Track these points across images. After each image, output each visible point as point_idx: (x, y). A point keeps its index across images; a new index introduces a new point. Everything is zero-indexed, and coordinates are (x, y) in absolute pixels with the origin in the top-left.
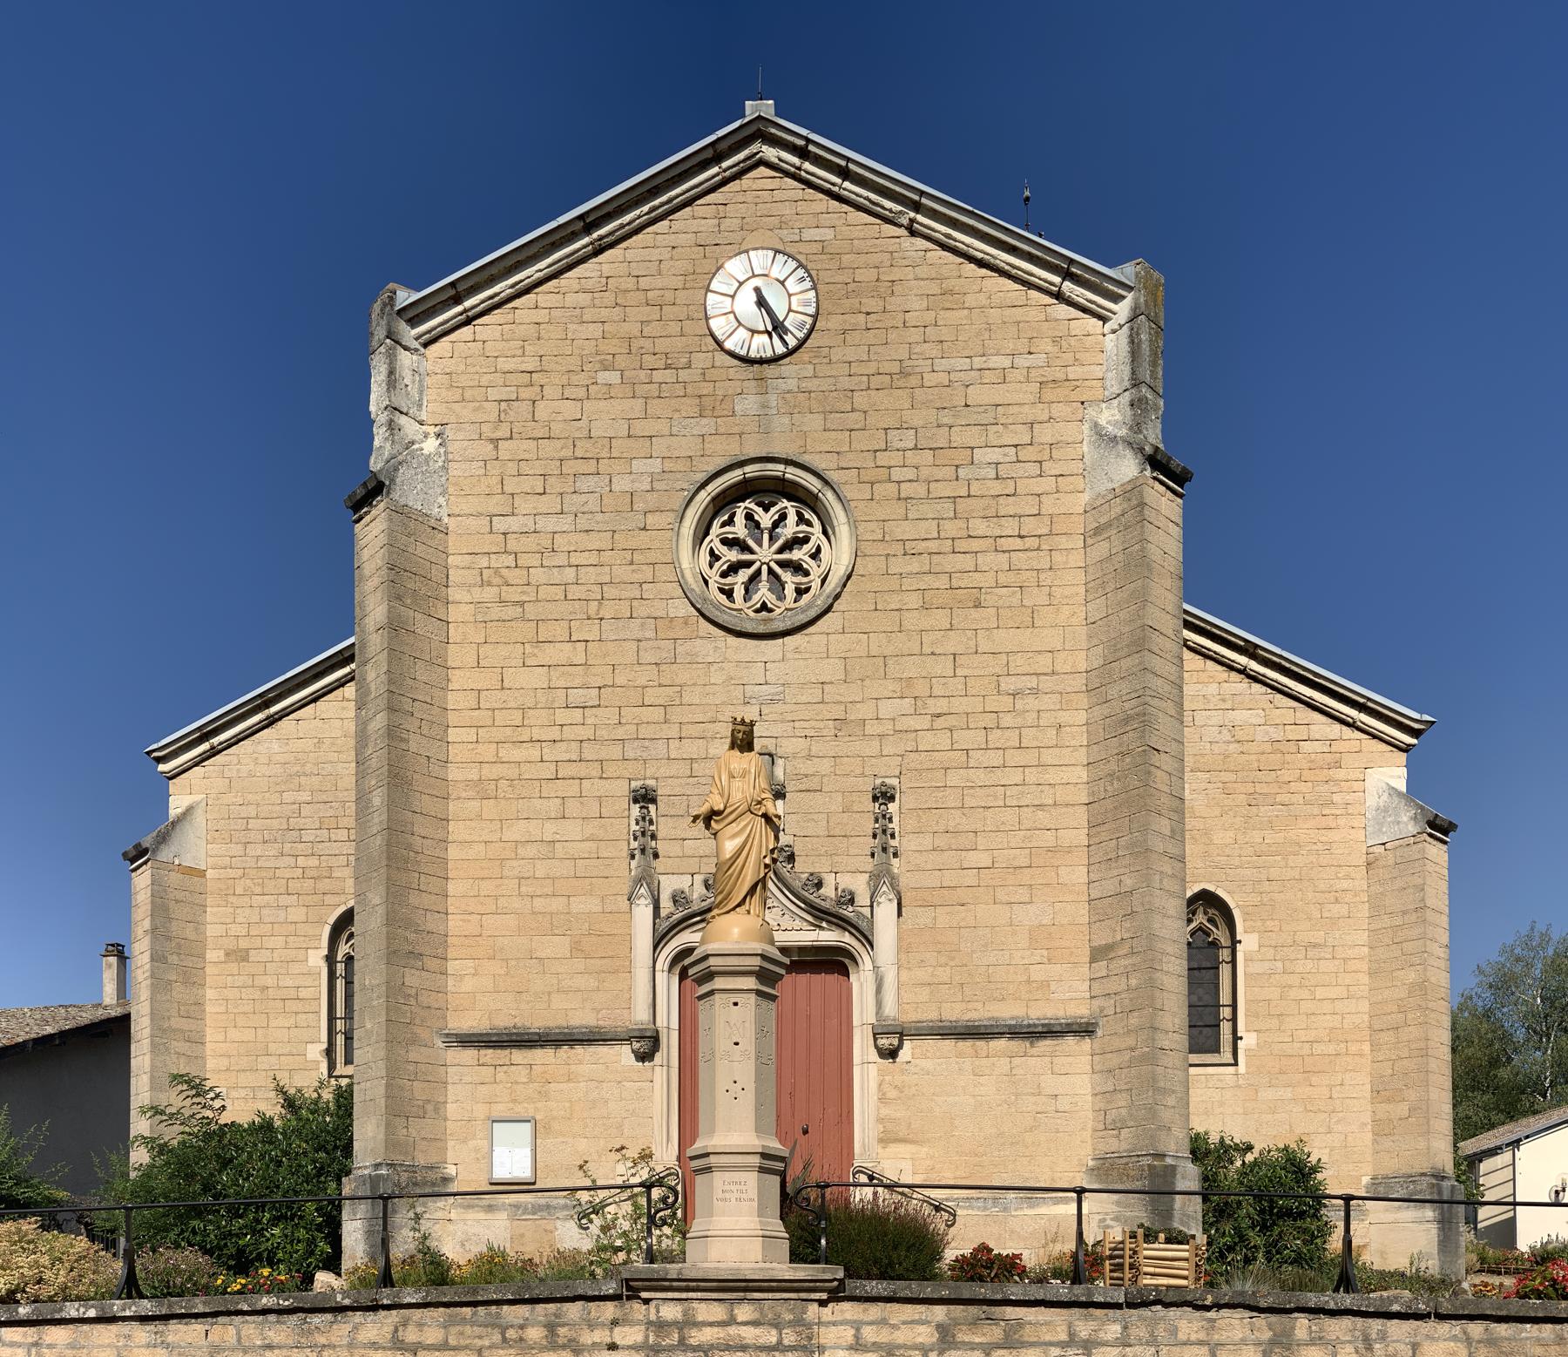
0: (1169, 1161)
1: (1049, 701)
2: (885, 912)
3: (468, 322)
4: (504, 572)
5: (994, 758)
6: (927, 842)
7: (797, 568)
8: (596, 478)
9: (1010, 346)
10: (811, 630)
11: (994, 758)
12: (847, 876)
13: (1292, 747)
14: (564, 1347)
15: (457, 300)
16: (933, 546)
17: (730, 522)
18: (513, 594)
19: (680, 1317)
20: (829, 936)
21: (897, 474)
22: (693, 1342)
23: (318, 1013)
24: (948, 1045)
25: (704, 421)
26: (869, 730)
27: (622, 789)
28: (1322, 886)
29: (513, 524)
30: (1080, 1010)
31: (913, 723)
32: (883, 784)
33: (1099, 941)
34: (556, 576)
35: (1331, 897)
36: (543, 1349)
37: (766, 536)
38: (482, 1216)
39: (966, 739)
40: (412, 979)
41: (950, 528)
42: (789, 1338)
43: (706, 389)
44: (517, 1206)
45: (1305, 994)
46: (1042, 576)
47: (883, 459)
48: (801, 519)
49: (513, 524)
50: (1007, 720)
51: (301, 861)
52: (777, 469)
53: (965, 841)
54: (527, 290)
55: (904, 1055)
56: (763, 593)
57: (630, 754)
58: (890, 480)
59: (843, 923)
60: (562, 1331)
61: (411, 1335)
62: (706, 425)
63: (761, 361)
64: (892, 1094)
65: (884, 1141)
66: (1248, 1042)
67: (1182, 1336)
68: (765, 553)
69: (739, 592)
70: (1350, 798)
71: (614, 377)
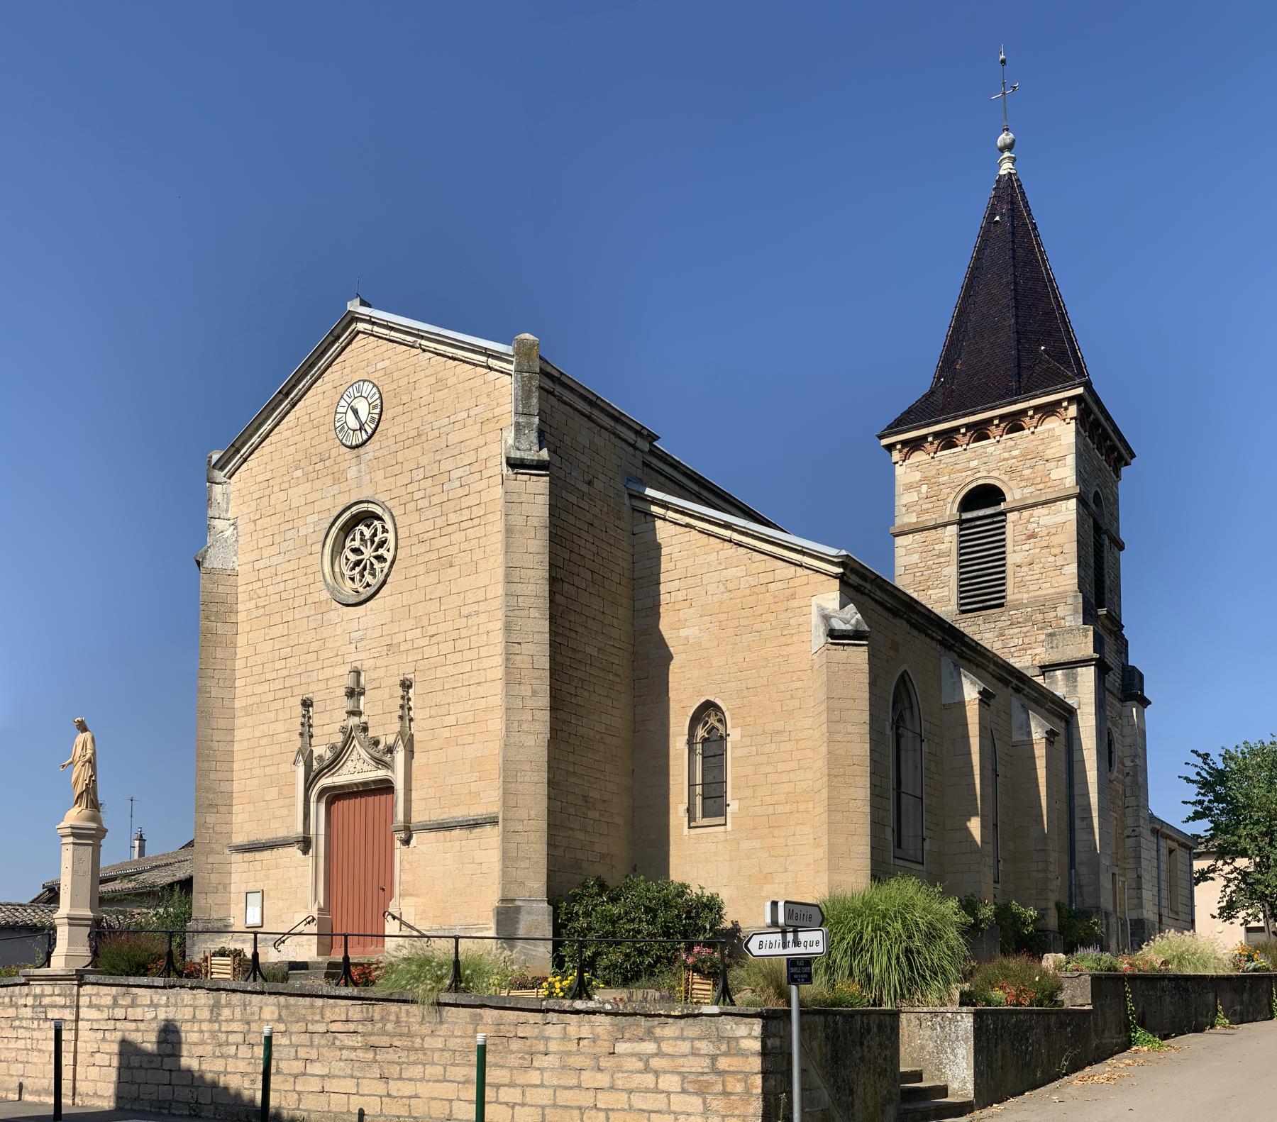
0: (518, 903)
1: (484, 617)
3: (245, 460)
6: (427, 713)
9: (467, 404)
13: (763, 589)
15: (238, 451)
16: (431, 535)
17: (353, 540)
27: (298, 701)
28: (782, 687)
35: (788, 695)
39: (446, 648)
40: (211, 819)
41: (440, 522)
45: (770, 769)
47: (411, 488)
53: (444, 710)
54: (267, 436)
55: (413, 842)
56: (368, 578)
63: (357, 446)
64: (407, 866)
66: (733, 807)
69: (357, 578)
70: (801, 620)
71: (299, 473)
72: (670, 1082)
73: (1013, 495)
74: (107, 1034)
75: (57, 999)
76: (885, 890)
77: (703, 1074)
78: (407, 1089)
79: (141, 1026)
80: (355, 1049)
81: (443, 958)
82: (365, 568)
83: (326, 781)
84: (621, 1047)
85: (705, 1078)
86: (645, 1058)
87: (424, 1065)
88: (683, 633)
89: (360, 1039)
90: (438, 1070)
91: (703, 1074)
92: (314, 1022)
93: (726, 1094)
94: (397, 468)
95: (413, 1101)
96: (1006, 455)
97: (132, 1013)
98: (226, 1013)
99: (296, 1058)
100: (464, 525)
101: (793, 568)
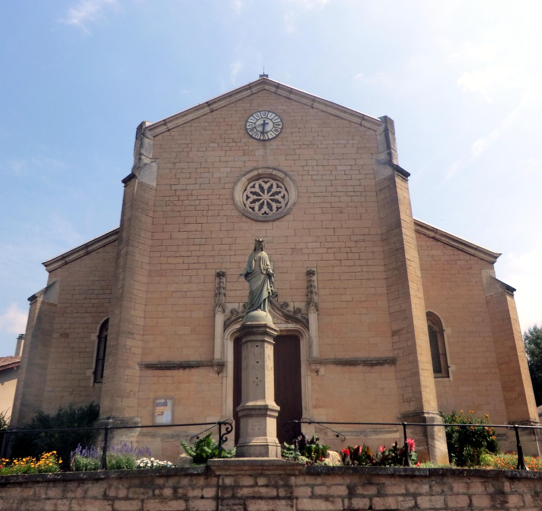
2: (313, 318)
4: (175, 202)
5: (351, 263)
7: (277, 201)
8: (207, 174)
10: (282, 220)
11: (351, 263)
12: (296, 303)
14: (180, 498)
16: (325, 194)
18: (177, 208)
19: (233, 484)
20: (291, 326)
21: (311, 173)
22: (239, 495)
23: (92, 357)
24: (339, 368)
25: (245, 157)
26: (304, 251)
27: (213, 272)
29: (179, 187)
30: (389, 354)
31: (320, 250)
32: (310, 270)
33: (395, 328)
34: (193, 203)
36: (172, 499)
38: (150, 439)
41: (330, 189)
42: (282, 493)
43: (246, 148)
44: (165, 435)
46: (363, 204)
47: (306, 168)
48: (278, 186)
49: (179, 187)
50: (354, 250)
51: (93, 301)
52: (270, 171)
56: (257, 205)
57: (216, 260)
58: (309, 175)
59: (296, 321)
60: (180, 491)
61: (112, 493)
62: (246, 158)
65: (315, 407)
68: (266, 197)
69: (250, 200)
71: (215, 145)
75: (263, 490)
76: (41, 507)
81: (239, 482)
94: (296, 157)
100: (350, 194)
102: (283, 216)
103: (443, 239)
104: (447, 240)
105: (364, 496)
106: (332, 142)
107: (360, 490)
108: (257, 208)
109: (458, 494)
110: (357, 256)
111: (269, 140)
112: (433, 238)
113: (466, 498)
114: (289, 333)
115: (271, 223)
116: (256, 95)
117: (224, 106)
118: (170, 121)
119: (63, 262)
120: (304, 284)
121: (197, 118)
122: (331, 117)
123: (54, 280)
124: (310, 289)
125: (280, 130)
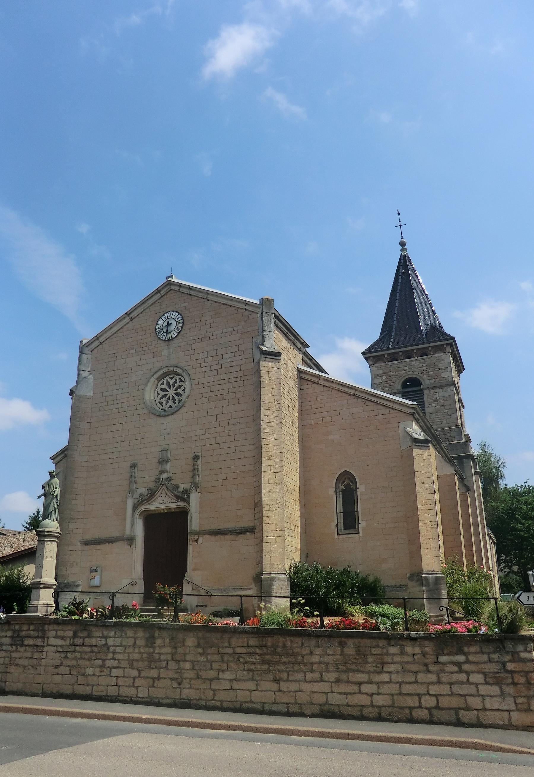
0: (273, 575)
5: (227, 445)
10: (178, 412)
11: (227, 445)
16: (211, 384)
20: (180, 504)
22: (21, 635)
24: (213, 538)
27: (128, 464)
37: (171, 386)
41: (217, 378)
42: (40, 635)
47: (199, 361)
48: (171, 378)
52: (171, 369)
59: (183, 500)
66: (363, 525)
67: (128, 635)
68: (171, 392)
71: (133, 351)
72: (477, 678)
73: (426, 382)
74: (69, 655)
75: (32, 632)
77: (498, 673)
78: (293, 687)
79: (95, 649)
80: (254, 663)
82: (169, 399)
83: (146, 507)
84: (443, 659)
85: (500, 675)
86: (458, 664)
87: (305, 673)
88: (330, 437)
89: (257, 657)
90: (317, 675)
91: (498, 673)
92: (223, 647)
93: (515, 684)
94: (191, 352)
95: (298, 694)
96: (421, 365)
97: (87, 641)
98: (159, 642)
99: (211, 669)
100: (231, 380)
101: (388, 409)
102: (180, 408)
103: (363, 395)
104: (367, 396)
105: (80, 637)
106: (221, 332)
107: (80, 634)
108: (164, 403)
109: (129, 637)
110: (232, 439)
111: (172, 339)
112: (354, 395)
113: (133, 640)
114: (180, 510)
115: (170, 417)
116: (165, 297)
117: (141, 313)
118: (101, 336)
119: (63, 455)
120: (191, 468)
121: (121, 328)
122: (223, 306)
123: (59, 470)
124: (194, 472)
125: (180, 328)
